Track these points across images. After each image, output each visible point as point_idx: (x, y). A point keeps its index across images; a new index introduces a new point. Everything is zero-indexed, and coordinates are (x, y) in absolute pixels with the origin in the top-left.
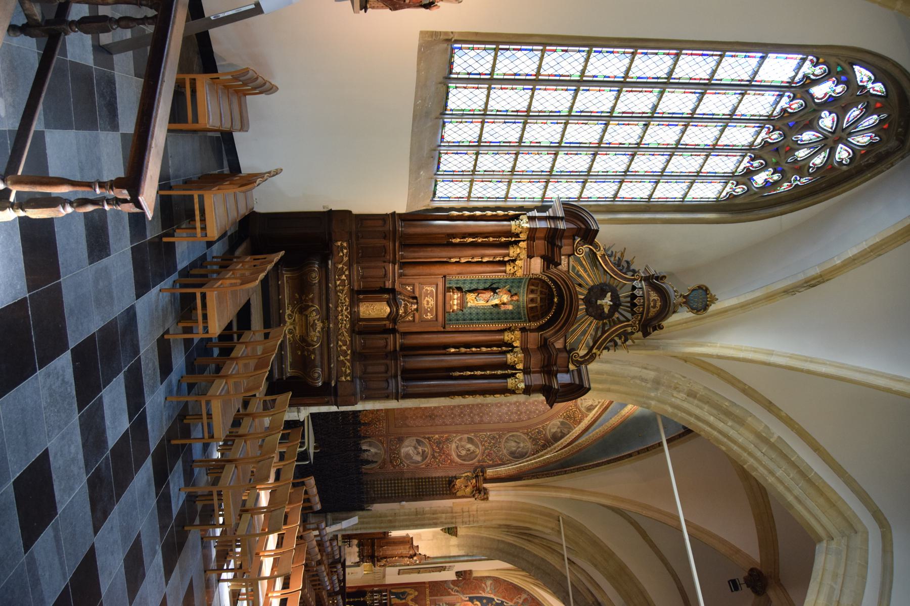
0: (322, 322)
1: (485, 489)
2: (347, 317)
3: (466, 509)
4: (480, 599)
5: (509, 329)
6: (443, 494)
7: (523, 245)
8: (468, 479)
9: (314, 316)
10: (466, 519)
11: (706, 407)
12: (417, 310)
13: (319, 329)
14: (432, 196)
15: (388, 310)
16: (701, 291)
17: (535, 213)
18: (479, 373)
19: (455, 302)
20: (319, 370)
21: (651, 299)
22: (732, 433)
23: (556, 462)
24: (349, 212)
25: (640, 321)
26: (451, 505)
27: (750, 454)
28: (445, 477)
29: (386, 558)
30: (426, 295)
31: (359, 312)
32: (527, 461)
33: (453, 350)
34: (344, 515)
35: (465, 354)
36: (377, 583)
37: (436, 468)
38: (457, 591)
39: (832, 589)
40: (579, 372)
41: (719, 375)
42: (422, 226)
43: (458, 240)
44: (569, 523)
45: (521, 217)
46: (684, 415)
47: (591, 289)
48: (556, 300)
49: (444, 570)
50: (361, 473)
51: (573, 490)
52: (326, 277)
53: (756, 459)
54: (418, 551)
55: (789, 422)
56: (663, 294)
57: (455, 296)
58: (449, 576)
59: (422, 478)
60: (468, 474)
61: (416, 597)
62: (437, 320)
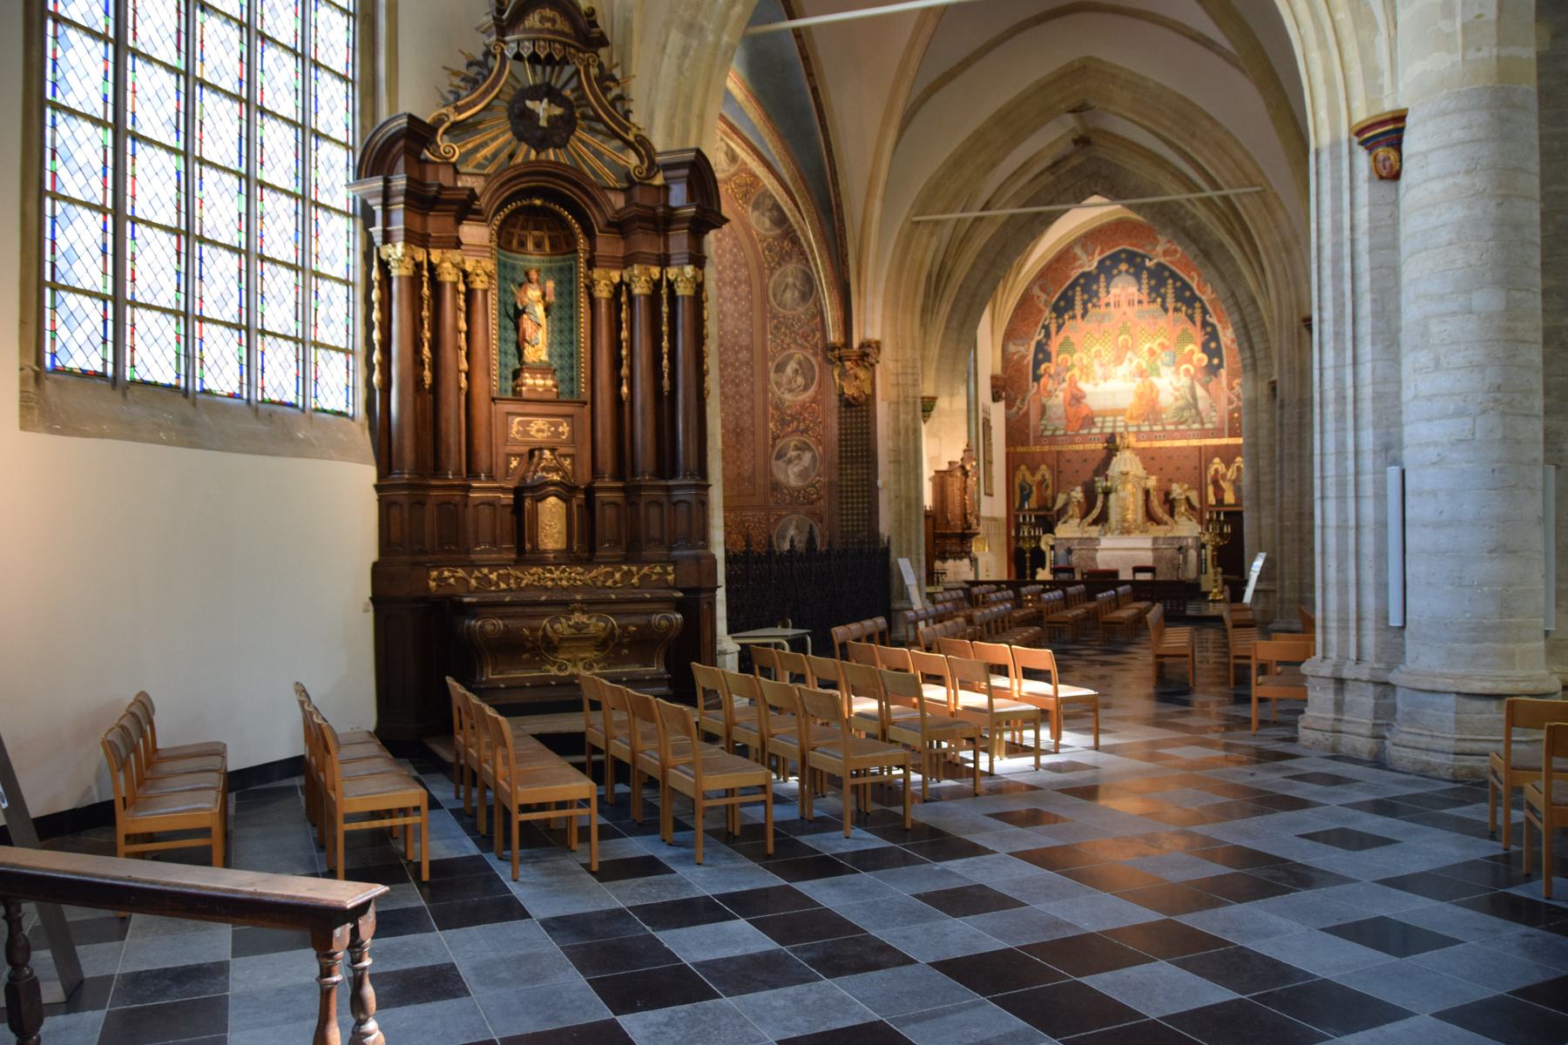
0: (572, 612)
1: (862, 346)
3: (893, 380)
5: (590, 288)
6: (867, 416)
7: (436, 256)
8: (844, 375)
9: (562, 627)
12: (552, 450)
14: (344, 419)
15: (552, 500)
18: (665, 344)
19: (540, 382)
20: (656, 618)
21: (538, 25)
25: (579, 50)
26: (885, 404)
28: (840, 412)
29: (965, 516)
30: (526, 433)
32: (818, 272)
33: (625, 389)
35: (631, 368)
38: (1023, 400)
40: (667, 167)
42: (401, 437)
44: (923, 206)
45: (384, 257)
47: (520, 137)
48: (538, 202)
51: (869, 194)
57: (529, 381)
59: (841, 452)
60: (836, 373)
61: (1029, 468)
62: (571, 416)
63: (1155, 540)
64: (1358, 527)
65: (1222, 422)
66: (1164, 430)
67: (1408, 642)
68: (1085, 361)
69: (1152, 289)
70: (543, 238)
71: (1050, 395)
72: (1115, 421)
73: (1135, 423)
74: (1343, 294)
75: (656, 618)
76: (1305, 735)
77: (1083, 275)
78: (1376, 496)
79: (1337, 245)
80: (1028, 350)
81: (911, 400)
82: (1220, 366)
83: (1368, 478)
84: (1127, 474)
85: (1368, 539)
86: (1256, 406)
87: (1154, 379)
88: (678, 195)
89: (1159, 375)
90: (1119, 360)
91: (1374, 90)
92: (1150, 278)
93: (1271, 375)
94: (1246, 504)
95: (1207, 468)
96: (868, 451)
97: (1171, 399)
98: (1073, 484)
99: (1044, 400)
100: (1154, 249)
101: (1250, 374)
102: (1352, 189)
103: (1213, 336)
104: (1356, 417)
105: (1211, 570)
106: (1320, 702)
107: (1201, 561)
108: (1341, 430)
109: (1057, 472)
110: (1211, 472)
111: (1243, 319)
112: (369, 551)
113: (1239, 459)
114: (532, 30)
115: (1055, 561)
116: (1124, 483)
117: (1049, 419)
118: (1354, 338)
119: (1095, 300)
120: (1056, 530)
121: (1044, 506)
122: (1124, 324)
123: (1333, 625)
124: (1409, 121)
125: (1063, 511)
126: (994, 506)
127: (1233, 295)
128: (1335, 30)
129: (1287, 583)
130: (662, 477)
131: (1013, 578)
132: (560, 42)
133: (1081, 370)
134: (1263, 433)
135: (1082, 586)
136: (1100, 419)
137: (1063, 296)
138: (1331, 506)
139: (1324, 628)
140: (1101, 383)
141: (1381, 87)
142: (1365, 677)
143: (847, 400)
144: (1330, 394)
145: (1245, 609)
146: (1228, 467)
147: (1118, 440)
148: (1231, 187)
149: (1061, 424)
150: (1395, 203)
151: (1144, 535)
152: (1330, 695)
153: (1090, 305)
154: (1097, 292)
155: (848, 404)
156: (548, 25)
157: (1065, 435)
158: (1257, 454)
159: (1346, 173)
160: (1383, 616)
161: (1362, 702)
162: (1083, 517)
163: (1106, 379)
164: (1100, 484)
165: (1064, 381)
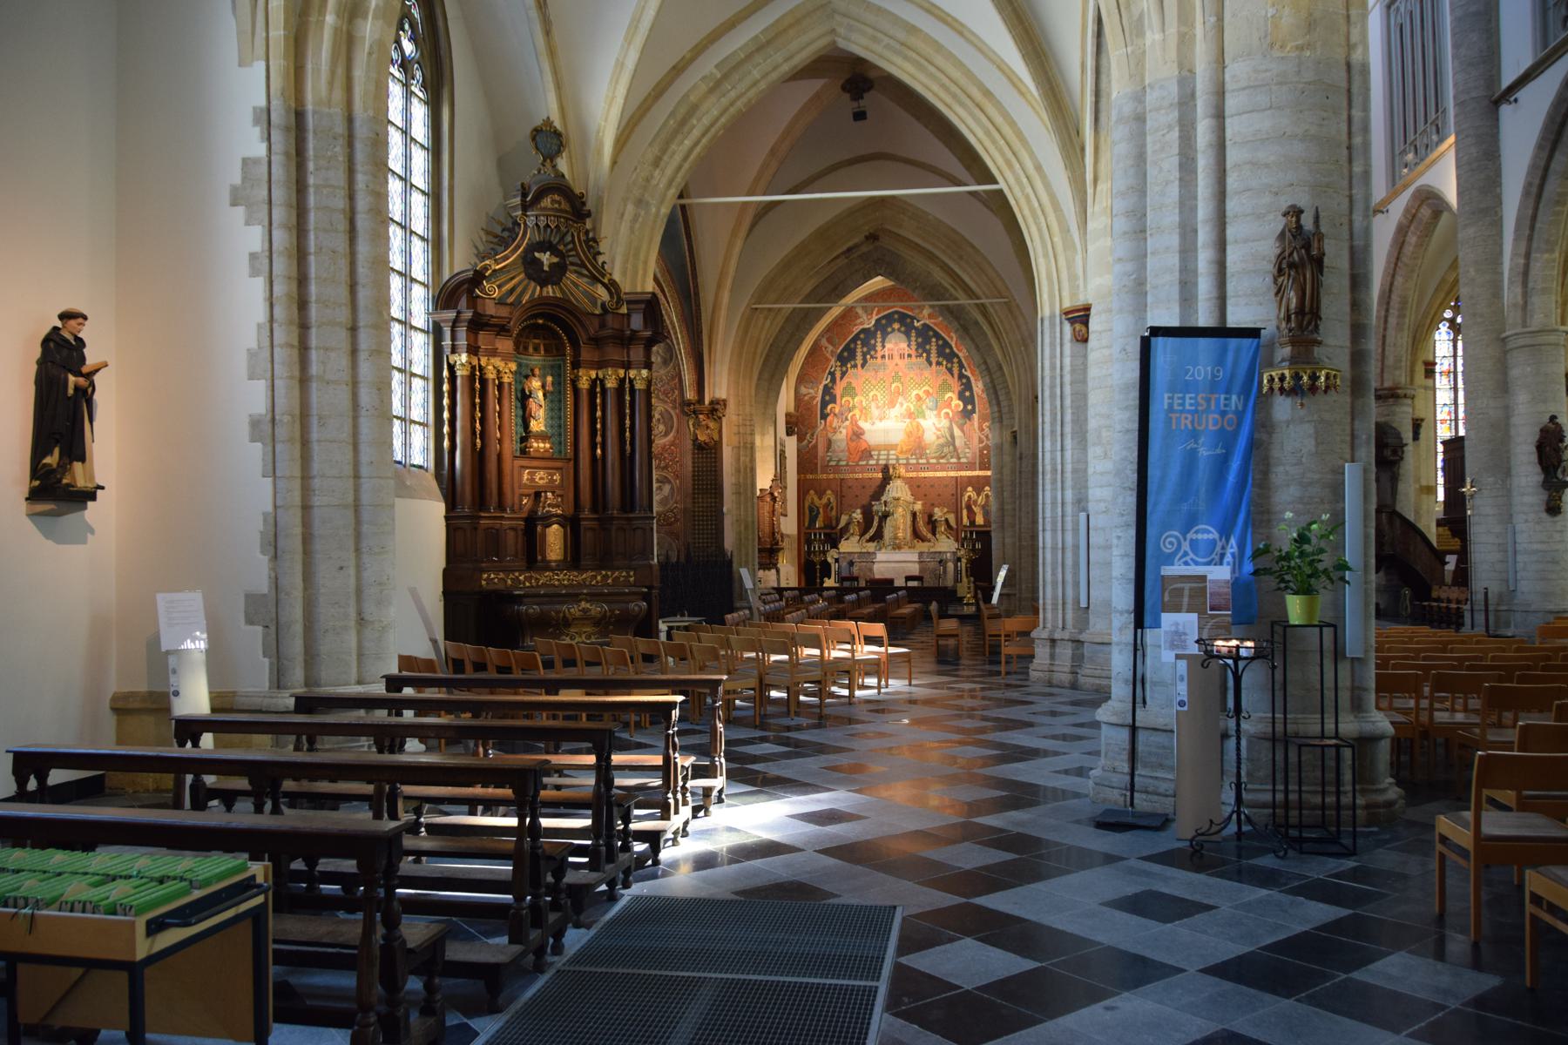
0: (580, 601)
1: (712, 403)
2: (565, 575)
3: (735, 429)
4: (824, 404)
5: (574, 382)
6: (715, 458)
7: (483, 361)
8: (697, 424)
9: (575, 610)
10: (748, 430)
11: (673, 147)
12: (553, 493)
13: (588, 605)
14: (422, 471)
15: (555, 526)
16: (538, 138)
17: (447, 342)
18: (628, 422)
19: (542, 445)
20: (632, 605)
21: (550, 206)
22: (706, 121)
23: (681, 305)
24: (445, 571)
25: (574, 222)
26: (730, 448)
27: (732, 104)
28: (694, 454)
29: (773, 534)
30: (532, 480)
31: (555, 561)
32: (678, 344)
33: (599, 451)
34: (736, 585)
35: (604, 436)
36: (796, 545)
37: (681, 466)
38: (812, 435)
39: (887, 47)
40: (629, 302)
41: (635, 125)
42: (463, 484)
43: (478, 440)
44: (761, 295)
45: (452, 362)
46: (680, 175)
47: (529, 277)
48: (541, 321)
49: (784, 452)
50: (677, 562)
51: (719, 286)
52: (533, 596)
53: (738, 98)
54: (766, 490)
55: (699, 50)
56: (542, 193)
57: (535, 445)
58: (791, 444)
59: (694, 485)
60: (691, 423)
61: (816, 492)
62: (561, 469)
63: (921, 554)
64: (1063, 549)
65: (974, 458)
66: (928, 463)
67: (1091, 617)
68: (864, 404)
69: (919, 346)
70: (539, 344)
71: (835, 431)
72: (888, 455)
73: (905, 456)
74: (1056, 408)
75: (632, 605)
76: (1033, 675)
77: (864, 331)
78: (1073, 530)
79: (1053, 378)
80: (817, 392)
81: (749, 446)
82: (973, 411)
83: (1069, 519)
84: (898, 499)
85: (1069, 554)
86: (1002, 449)
87: (921, 421)
88: (637, 322)
89: (924, 417)
90: (892, 404)
91: (1073, 295)
92: (917, 337)
93: (1013, 426)
94: (994, 526)
95: (962, 495)
96: (716, 484)
97: (934, 438)
98: (852, 508)
99: (830, 435)
100: (921, 312)
101: (997, 425)
102: (1062, 345)
103: (968, 386)
104: (1062, 482)
105: (965, 579)
106: (1042, 653)
107: (957, 571)
108: (1054, 489)
109: (841, 497)
110: (966, 498)
111: (992, 381)
112: (441, 562)
113: (987, 488)
114: (545, 209)
115: (838, 573)
116: (896, 507)
117: (834, 451)
118: (1062, 435)
119: (872, 353)
120: (840, 546)
121: (830, 525)
122: (897, 373)
123: (1049, 607)
124: (1093, 311)
125: (845, 530)
126: (789, 525)
127: (985, 363)
128: (1053, 248)
129: (1024, 587)
130: (626, 512)
131: (803, 585)
132: (564, 218)
133: (861, 411)
134: (1007, 471)
135: (868, 592)
136: (876, 453)
137: (847, 348)
138: (1048, 535)
139: (1044, 609)
140: (877, 422)
141: (1078, 286)
142: (1067, 638)
143: (700, 444)
144: (1048, 468)
145: (993, 607)
146: (978, 495)
147: (891, 470)
148: (987, 297)
149: (844, 455)
150: (1085, 356)
151: (912, 550)
152: (1047, 650)
153: (868, 357)
154: (875, 346)
155: (700, 447)
156: (556, 206)
157: (847, 465)
158: (1002, 487)
159: (1058, 335)
160: (1077, 601)
161: (1065, 652)
162: (862, 535)
163: (881, 420)
164: (878, 507)
165: (847, 419)
